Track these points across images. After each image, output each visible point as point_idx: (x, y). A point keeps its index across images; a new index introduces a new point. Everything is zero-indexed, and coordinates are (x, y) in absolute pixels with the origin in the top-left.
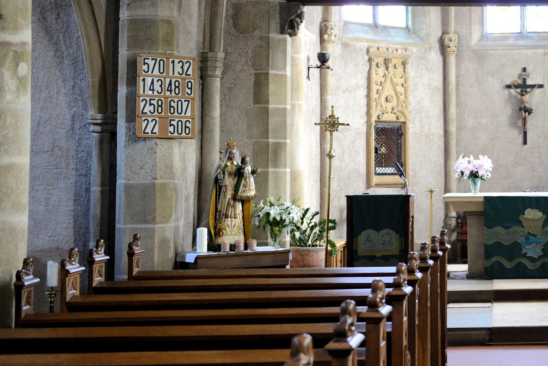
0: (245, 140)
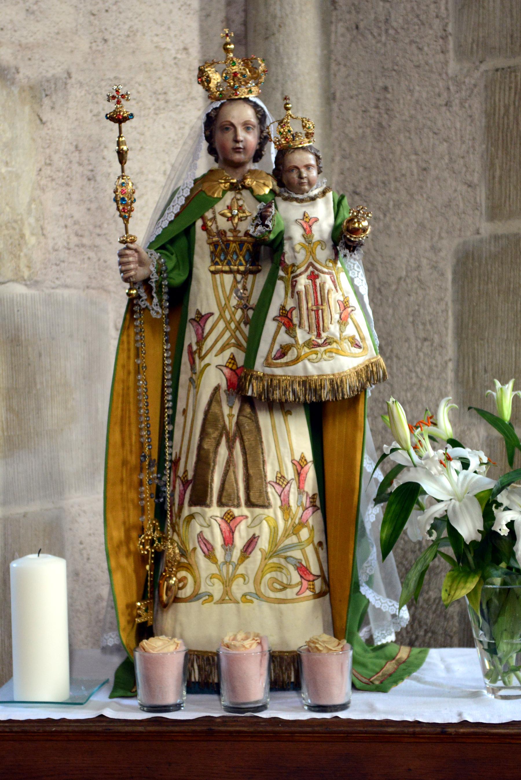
0: (453, 67)
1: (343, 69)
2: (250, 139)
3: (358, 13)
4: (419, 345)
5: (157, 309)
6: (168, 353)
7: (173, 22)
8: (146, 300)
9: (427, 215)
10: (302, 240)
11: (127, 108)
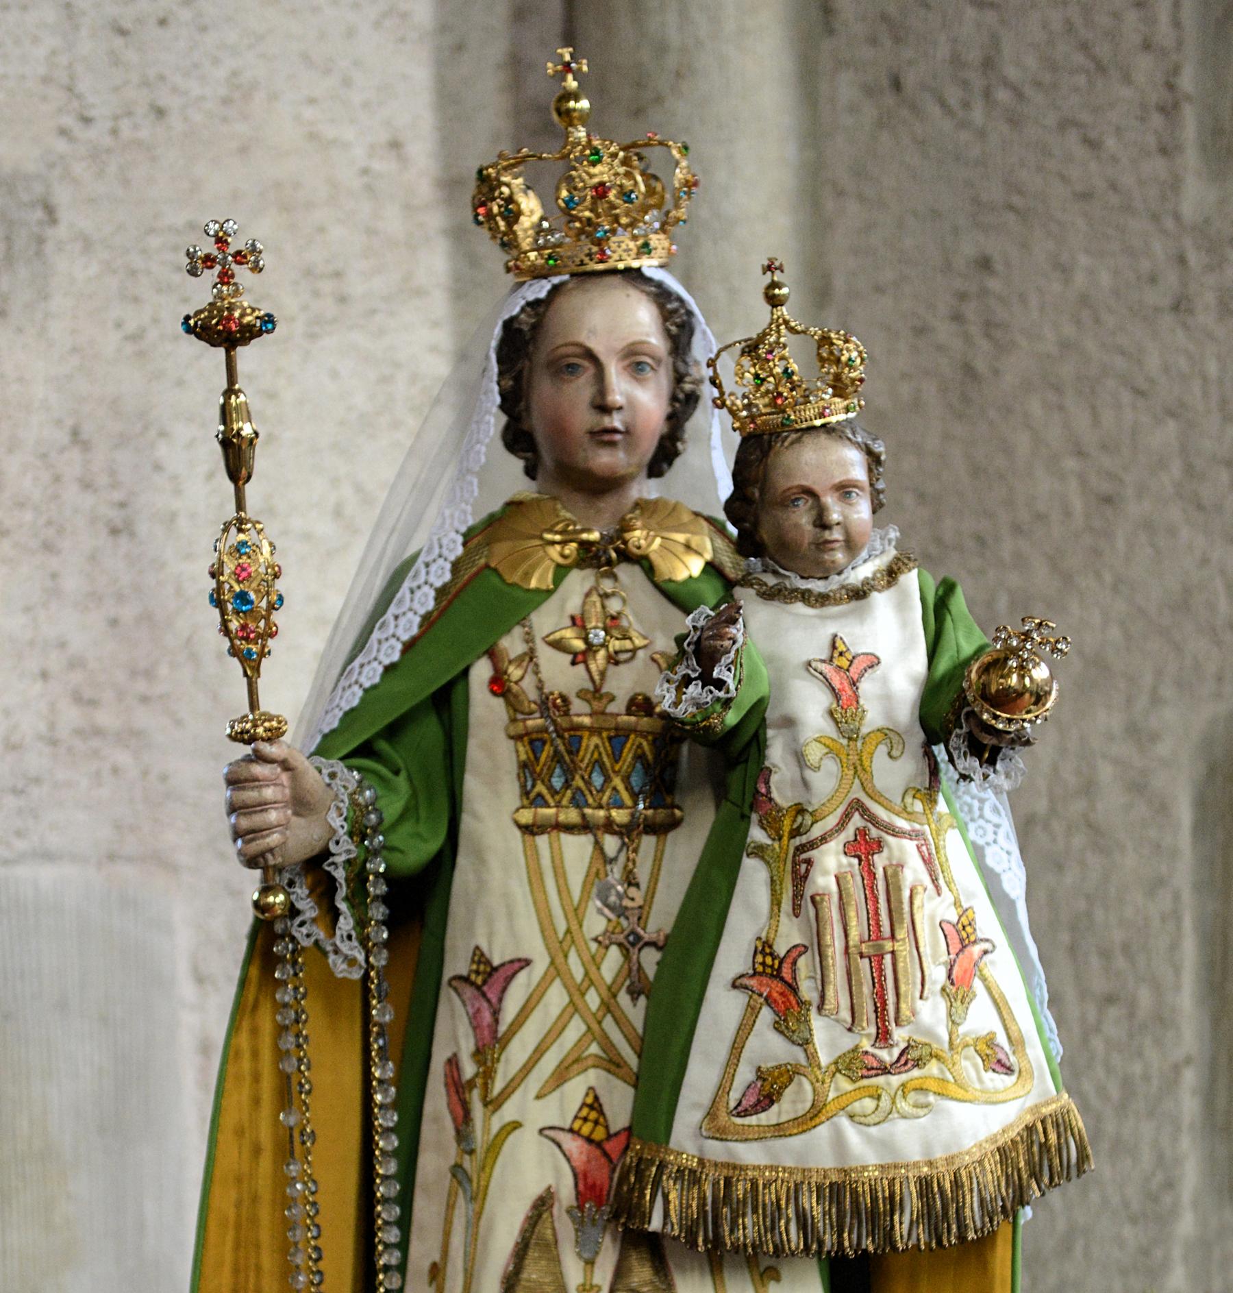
0: (1196, 196)
1: (853, 207)
2: (645, 401)
3: (897, 40)
4: (1092, 1015)
5: (348, 952)
6: (385, 1092)
7: (356, 63)
8: (314, 920)
9: (1115, 633)
10: (829, 729)
11: (253, 294)
